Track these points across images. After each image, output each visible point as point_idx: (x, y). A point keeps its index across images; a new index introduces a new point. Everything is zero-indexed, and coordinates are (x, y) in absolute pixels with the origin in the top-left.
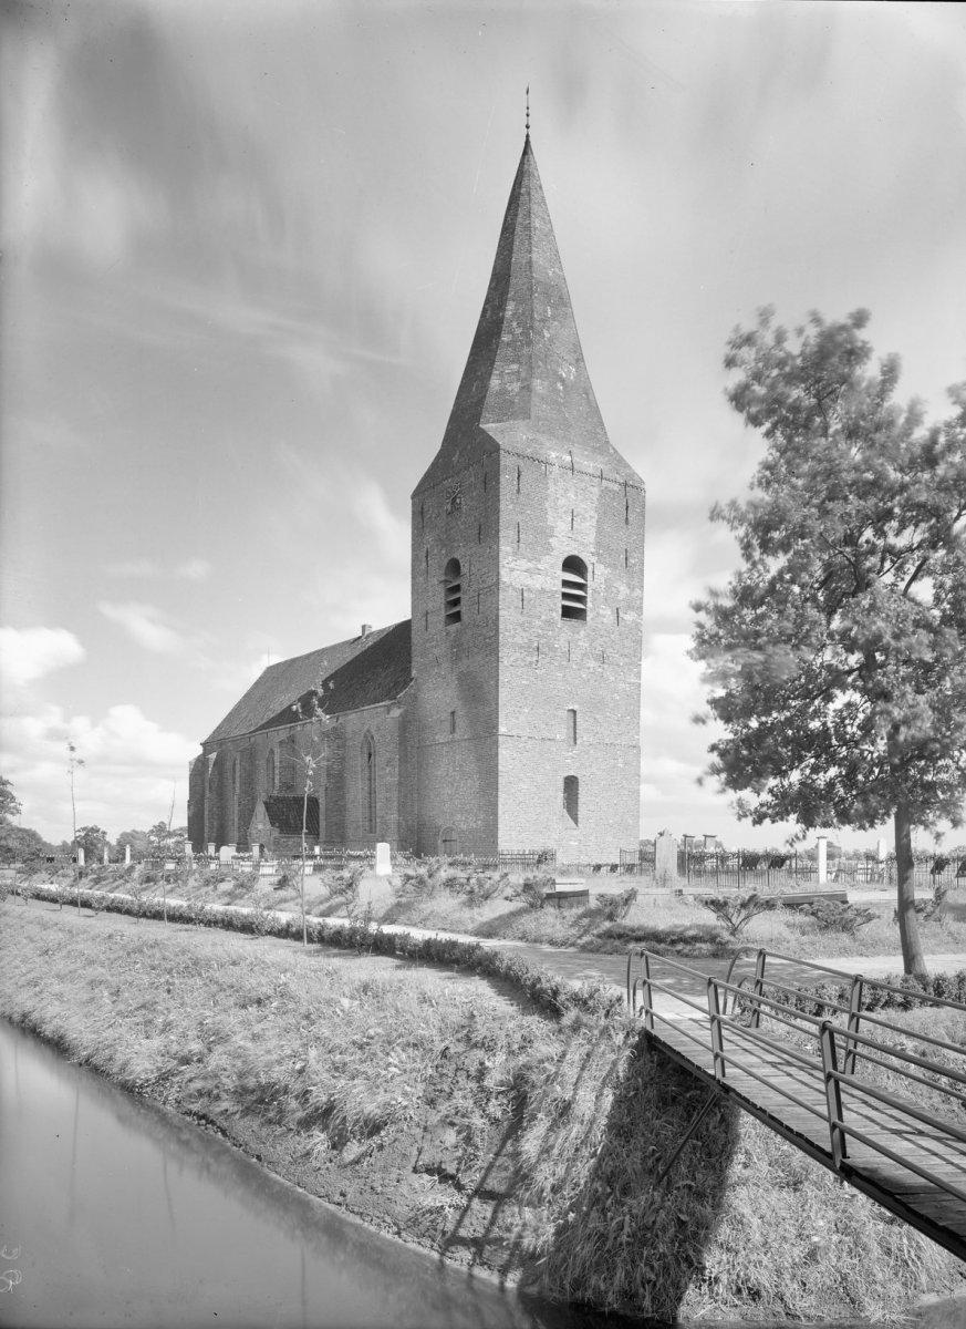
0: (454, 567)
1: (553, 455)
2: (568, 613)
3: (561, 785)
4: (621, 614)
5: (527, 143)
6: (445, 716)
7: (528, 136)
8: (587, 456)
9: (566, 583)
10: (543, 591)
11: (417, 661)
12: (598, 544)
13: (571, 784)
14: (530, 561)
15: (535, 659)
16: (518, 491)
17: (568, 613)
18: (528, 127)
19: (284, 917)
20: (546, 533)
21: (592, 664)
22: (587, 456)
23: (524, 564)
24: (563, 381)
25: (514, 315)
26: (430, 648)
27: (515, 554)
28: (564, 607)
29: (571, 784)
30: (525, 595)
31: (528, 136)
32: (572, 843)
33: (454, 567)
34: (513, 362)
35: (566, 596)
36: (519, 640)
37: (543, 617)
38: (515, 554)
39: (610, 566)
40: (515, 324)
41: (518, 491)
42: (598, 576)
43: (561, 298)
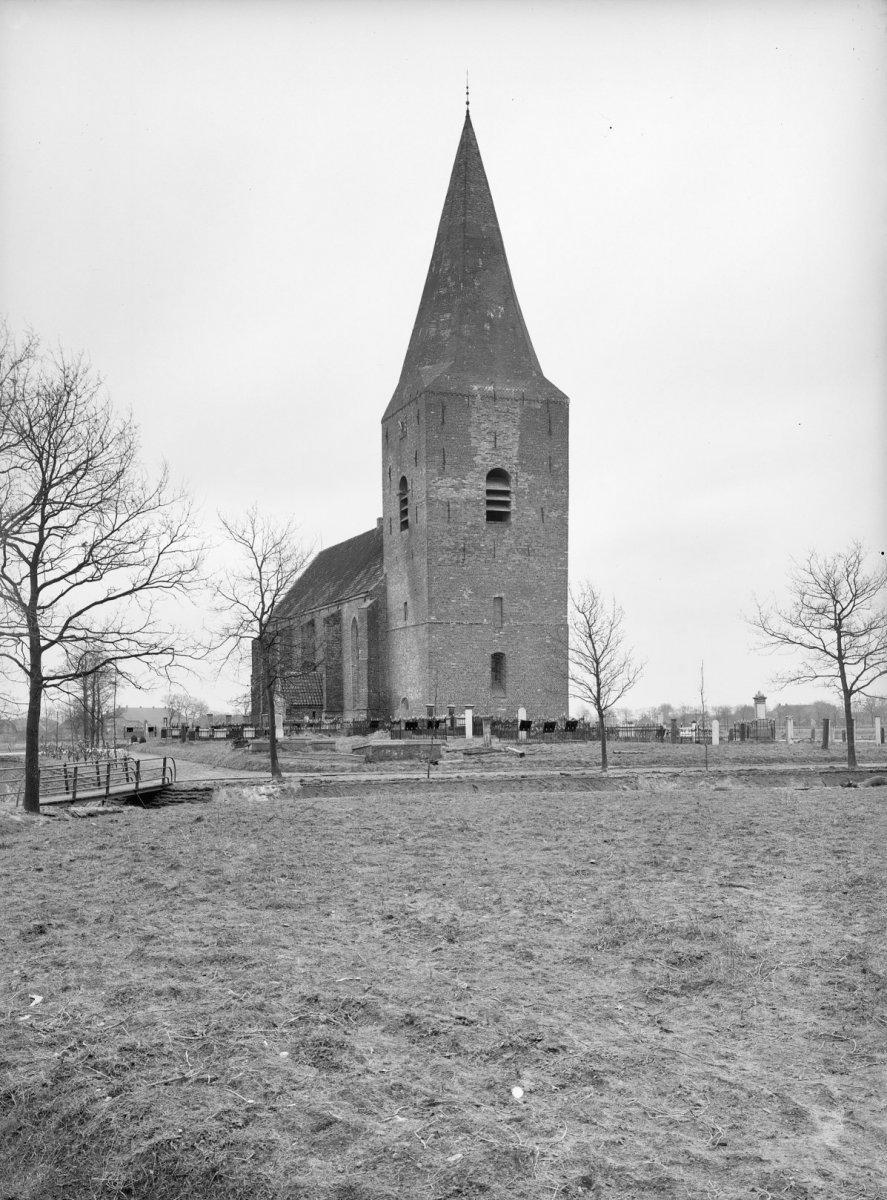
0: (404, 481)
1: (476, 388)
2: (493, 517)
3: (489, 661)
4: (546, 513)
5: (468, 116)
6: (402, 606)
7: (468, 111)
8: (509, 384)
9: (489, 492)
10: (468, 501)
11: (387, 558)
12: (521, 455)
13: (498, 660)
14: (455, 478)
15: (461, 557)
16: (443, 423)
17: (493, 517)
18: (468, 103)
19: (373, 798)
20: (471, 453)
21: (517, 557)
22: (509, 384)
23: (449, 481)
24: (490, 320)
25: (449, 271)
26: (394, 541)
27: (440, 474)
28: (488, 513)
29: (498, 660)
30: (451, 506)
31: (468, 111)
32: (499, 709)
33: (404, 481)
34: (446, 312)
35: (489, 503)
36: (445, 544)
37: (469, 523)
38: (440, 474)
39: (534, 472)
40: (449, 279)
41: (443, 423)
42: (521, 482)
43: (493, 248)
